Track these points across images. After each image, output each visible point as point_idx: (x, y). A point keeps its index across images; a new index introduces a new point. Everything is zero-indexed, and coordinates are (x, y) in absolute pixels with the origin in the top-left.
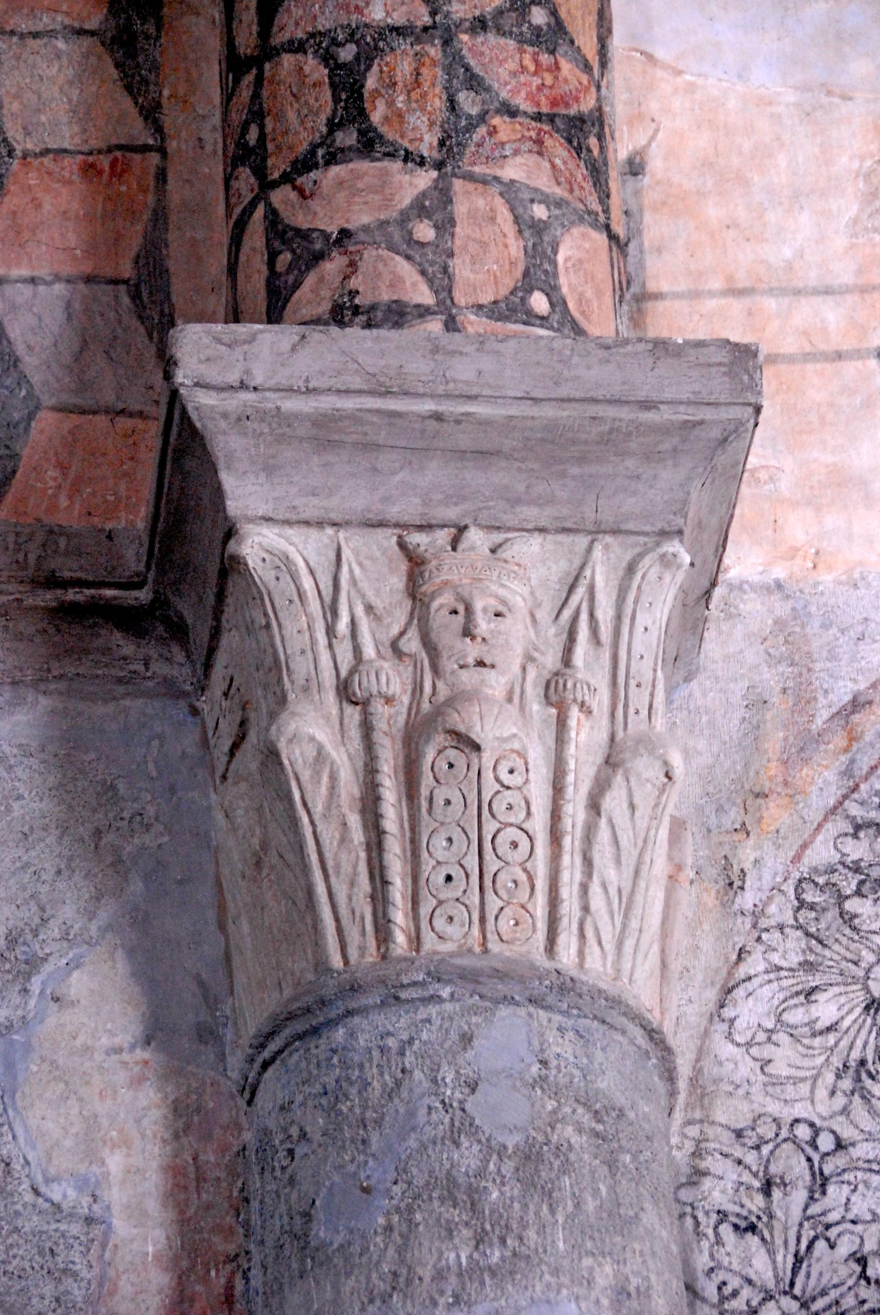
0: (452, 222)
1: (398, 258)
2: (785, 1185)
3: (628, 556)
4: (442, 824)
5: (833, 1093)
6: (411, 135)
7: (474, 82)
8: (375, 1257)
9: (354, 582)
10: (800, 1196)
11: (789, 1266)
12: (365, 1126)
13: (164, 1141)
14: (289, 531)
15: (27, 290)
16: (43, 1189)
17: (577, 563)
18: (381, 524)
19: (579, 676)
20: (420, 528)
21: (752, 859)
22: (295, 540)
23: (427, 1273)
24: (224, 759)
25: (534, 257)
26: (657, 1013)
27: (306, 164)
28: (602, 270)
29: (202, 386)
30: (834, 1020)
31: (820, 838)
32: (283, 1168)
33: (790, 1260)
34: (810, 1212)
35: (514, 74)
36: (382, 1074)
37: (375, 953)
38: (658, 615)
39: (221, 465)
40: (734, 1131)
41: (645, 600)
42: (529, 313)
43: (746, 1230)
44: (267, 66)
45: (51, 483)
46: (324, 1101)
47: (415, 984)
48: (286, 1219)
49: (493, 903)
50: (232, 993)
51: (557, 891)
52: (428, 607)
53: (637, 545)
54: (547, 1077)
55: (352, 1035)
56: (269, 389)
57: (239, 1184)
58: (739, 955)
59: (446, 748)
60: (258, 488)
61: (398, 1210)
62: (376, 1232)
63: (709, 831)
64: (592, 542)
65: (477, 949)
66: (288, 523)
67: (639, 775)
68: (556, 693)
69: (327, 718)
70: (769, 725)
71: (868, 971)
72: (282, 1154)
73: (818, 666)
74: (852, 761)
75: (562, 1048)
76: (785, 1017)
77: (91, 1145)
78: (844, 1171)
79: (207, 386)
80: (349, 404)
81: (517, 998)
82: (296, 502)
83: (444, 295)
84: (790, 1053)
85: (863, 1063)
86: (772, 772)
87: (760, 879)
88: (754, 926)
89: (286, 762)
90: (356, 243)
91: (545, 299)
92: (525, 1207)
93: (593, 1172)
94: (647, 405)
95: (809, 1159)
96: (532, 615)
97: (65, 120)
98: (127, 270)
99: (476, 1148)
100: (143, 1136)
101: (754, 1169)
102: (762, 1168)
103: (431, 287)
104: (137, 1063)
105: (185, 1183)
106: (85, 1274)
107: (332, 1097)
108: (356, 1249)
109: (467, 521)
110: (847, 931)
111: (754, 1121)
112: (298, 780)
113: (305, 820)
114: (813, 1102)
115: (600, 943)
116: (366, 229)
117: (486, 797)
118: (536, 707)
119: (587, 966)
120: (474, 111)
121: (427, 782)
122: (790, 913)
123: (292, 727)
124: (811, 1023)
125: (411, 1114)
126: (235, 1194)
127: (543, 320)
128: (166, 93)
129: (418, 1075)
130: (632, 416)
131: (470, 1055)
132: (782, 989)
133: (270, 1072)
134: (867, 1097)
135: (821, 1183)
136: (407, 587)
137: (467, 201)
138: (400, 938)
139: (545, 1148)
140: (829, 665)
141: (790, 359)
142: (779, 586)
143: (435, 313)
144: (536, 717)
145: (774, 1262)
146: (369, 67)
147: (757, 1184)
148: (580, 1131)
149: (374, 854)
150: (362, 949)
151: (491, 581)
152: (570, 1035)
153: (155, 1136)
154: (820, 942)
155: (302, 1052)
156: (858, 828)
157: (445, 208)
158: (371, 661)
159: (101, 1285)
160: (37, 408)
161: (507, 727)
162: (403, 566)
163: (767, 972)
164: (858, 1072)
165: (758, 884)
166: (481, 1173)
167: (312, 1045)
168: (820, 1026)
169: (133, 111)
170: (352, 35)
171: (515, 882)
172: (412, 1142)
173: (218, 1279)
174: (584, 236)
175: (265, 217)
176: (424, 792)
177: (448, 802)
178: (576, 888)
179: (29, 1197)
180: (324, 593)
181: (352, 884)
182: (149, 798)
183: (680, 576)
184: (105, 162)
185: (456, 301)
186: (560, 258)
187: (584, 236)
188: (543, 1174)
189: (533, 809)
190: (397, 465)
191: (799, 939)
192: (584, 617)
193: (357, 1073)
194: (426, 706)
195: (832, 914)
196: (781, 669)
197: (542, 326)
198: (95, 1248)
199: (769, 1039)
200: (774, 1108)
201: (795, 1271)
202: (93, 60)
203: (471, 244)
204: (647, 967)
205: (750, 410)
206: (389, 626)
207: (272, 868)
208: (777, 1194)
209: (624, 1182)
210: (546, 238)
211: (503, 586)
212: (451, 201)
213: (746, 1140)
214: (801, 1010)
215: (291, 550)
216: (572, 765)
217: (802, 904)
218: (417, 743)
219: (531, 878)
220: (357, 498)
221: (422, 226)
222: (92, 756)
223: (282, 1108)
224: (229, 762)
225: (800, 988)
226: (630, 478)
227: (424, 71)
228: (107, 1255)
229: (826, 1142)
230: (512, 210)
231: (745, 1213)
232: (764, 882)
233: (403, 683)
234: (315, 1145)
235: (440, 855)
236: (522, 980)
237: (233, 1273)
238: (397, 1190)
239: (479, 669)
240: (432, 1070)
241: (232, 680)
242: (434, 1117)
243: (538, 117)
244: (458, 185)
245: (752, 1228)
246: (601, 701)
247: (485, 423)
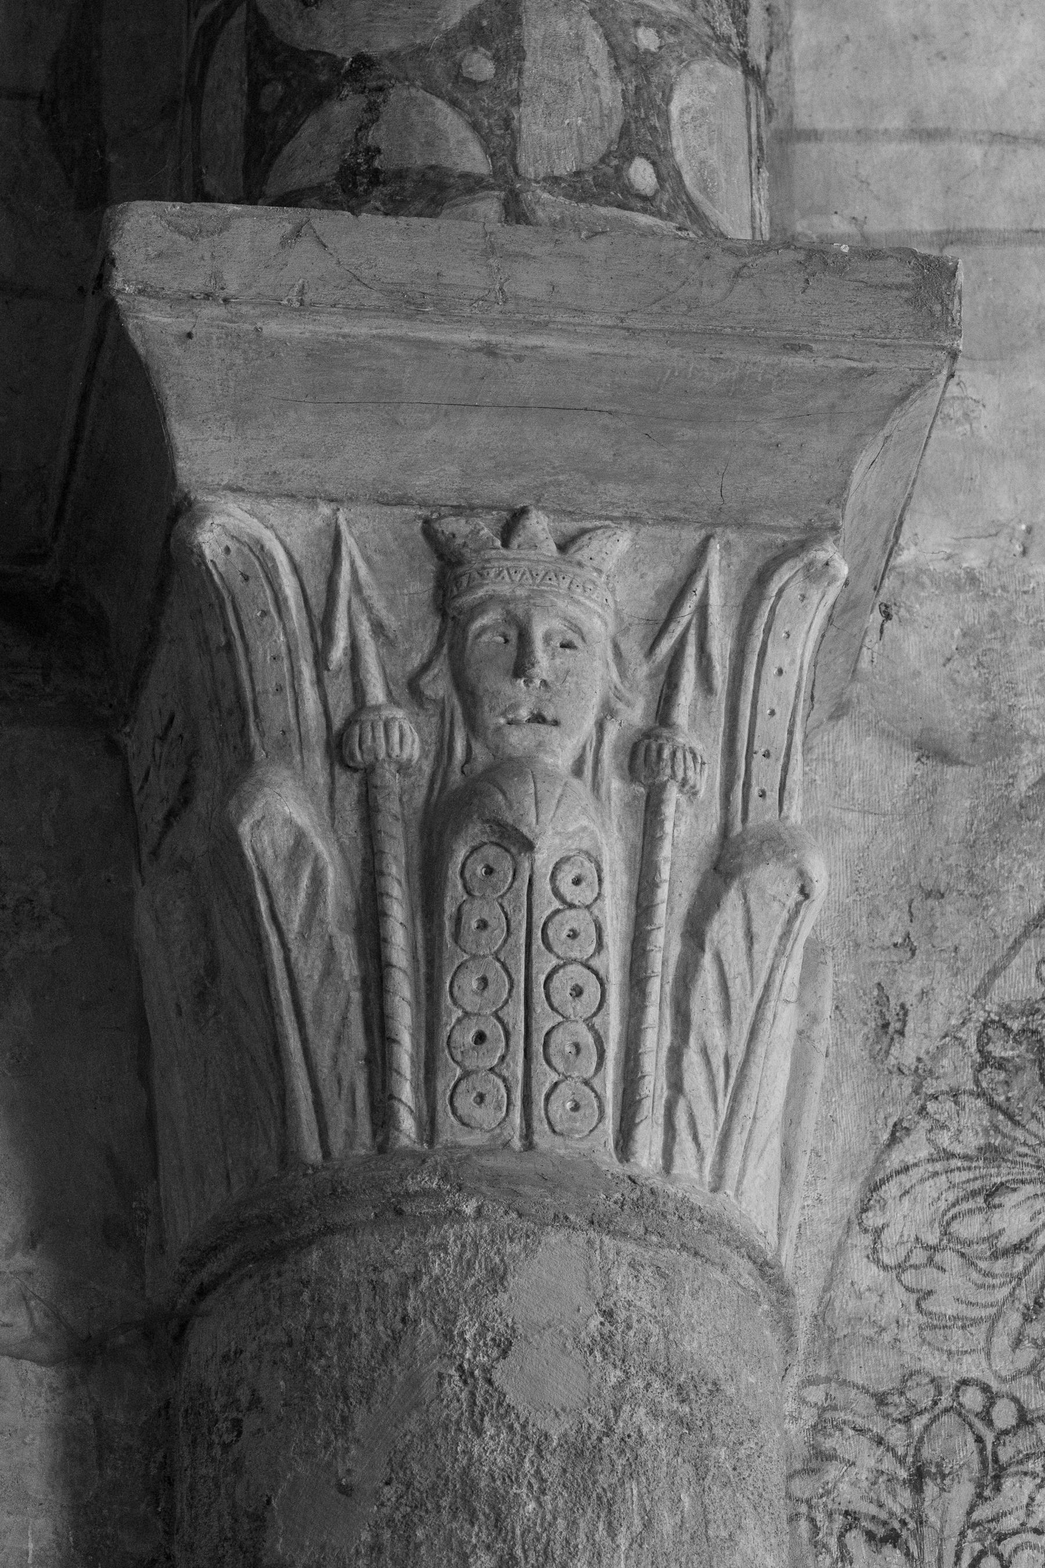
0: (520, 53)
1: (439, 104)
2: (944, 1477)
4: (474, 957)
5: (1017, 1343)
9: (357, 587)
10: (963, 1492)
12: (346, 1398)
13: (52, 1389)
14: (265, 507)
17: (683, 570)
18: (401, 502)
19: (681, 740)
20: (458, 511)
21: (917, 989)
22: (273, 520)
24: (156, 829)
25: (636, 107)
26: (773, 1238)
28: (734, 124)
30: (1025, 1234)
31: (1017, 961)
32: (226, 1447)
34: (975, 1516)
36: (373, 1322)
37: (368, 1142)
38: (799, 651)
40: (874, 1395)
41: (780, 629)
43: (884, 1540)
46: (287, 1355)
47: (425, 1193)
48: (227, 1521)
49: (544, 1077)
50: (155, 1175)
52: (465, 631)
54: (611, 1335)
55: (330, 1262)
57: (159, 1456)
58: (893, 1134)
59: (483, 844)
60: (224, 444)
62: (358, 1552)
63: (857, 945)
65: (517, 1143)
66: (264, 495)
67: (762, 891)
68: (645, 759)
69: (311, 791)
70: (950, 787)
73: (1024, 702)
76: (955, 1227)
78: (1028, 1457)
80: (362, 329)
81: (572, 1217)
82: (278, 466)
83: (504, 160)
84: (959, 1281)
86: (952, 861)
87: (928, 1020)
88: (916, 1091)
89: (249, 854)
90: (379, 77)
91: (650, 170)
92: (572, 1525)
93: (672, 1475)
95: (979, 1439)
101: (900, 1451)
102: (912, 1452)
103: (486, 149)
104: (16, 1274)
111: (904, 1381)
113: (274, 940)
114: (988, 1354)
116: (393, 56)
117: (540, 918)
118: (614, 785)
119: (675, 1171)
121: (454, 892)
125: (414, 1383)
126: (154, 1471)
127: (646, 202)
131: (502, 1299)
132: (952, 1186)
136: (435, 596)
138: (407, 1123)
139: (606, 1441)
141: (1002, 240)
142: (973, 579)
143: (490, 187)
144: (615, 798)
147: (903, 1474)
148: (655, 1414)
149: (372, 996)
150: (351, 1135)
151: (558, 595)
153: (40, 1383)
154: (1010, 1117)
155: (257, 1279)
157: (510, 32)
158: (377, 708)
161: (576, 827)
162: (431, 567)
163: (931, 1160)
165: (924, 1028)
167: (273, 1272)
172: (413, 1425)
174: (709, 73)
175: (248, 27)
176: (450, 908)
178: (664, 1053)
180: (313, 601)
181: (339, 1039)
182: (44, 876)
183: (833, 592)
185: (521, 171)
186: (674, 109)
187: (709, 73)
188: (601, 1478)
190: (427, 416)
191: (980, 1112)
192: (691, 650)
193: (336, 1317)
194: (456, 778)
196: (970, 704)
197: (644, 211)
199: (931, 1260)
200: (933, 1362)
203: (545, 85)
204: (761, 1171)
208: (931, 1489)
209: (715, 1489)
210: (655, 79)
212: (519, 22)
213: (891, 1410)
214: (979, 1218)
216: (665, 871)
217: (986, 1060)
218: (441, 834)
221: (476, 56)
223: (225, 1358)
224: (163, 834)
225: (977, 1185)
229: (1004, 1415)
230: (607, 36)
231: (883, 1515)
232: (934, 1025)
233: (423, 741)
239: (536, 726)
240: (446, 1320)
241: (172, 719)
245: (893, 1538)
246: (708, 780)
247: (557, 362)
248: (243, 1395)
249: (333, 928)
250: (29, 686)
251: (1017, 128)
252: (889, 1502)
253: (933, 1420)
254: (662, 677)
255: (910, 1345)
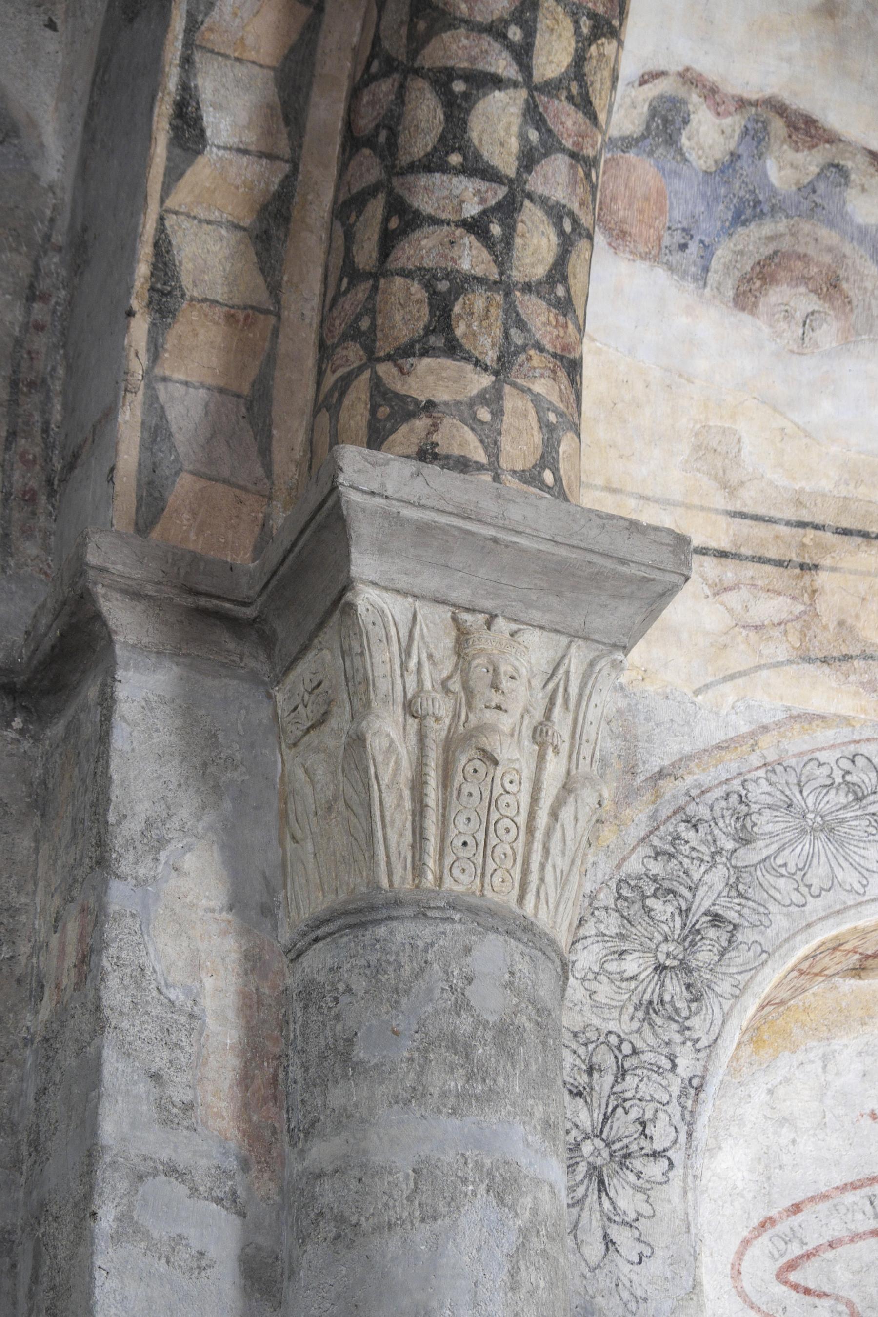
0: (502, 412)
1: (466, 428)
3: (591, 656)
5: (632, 1019)
6: (480, 349)
7: (521, 324)
8: (401, 1076)
9: (422, 637)
10: (609, 1079)
11: (601, 1121)
12: (398, 993)
14: (385, 594)
15: (182, 389)
16: (164, 990)
17: (560, 654)
18: (444, 602)
20: (468, 610)
22: (388, 601)
23: (436, 1092)
27: (407, 351)
29: (354, 488)
31: (634, 856)
33: (601, 1117)
34: (614, 1090)
35: (544, 324)
36: (411, 961)
39: (353, 543)
42: (543, 482)
43: (576, 1094)
44: (382, 281)
45: (185, 522)
46: (368, 972)
47: (437, 908)
48: (331, 1041)
49: (491, 866)
51: (528, 865)
52: (470, 663)
53: (597, 650)
56: (395, 499)
57: (283, 1010)
61: (418, 1049)
64: (571, 642)
65: (478, 893)
66: (386, 589)
67: (583, 800)
68: (540, 734)
71: (658, 946)
72: (329, 999)
73: (640, 744)
74: (657, 810)
75: (523, 966)
76: (606, 965)
77: (195, 967)
79: (357, 489)
80: (443, 519)
82: (394, 576)
85: (651, 1003)
88: (590, 905)
89: (369, 747)
94: (623, 561)
95: (616, 1057)
96: (529, 682)
97: (220, 282)
98: (246, 389)
99: (471, 1020)
100: (226, 969)
103: (486, 451)
105: (251, 1004)
106: (187, 1048)
107: (375, 971)
108: (387, 1068)
109: (498, 612)
110: (646, 918)
112: (374, 760)
115: (547, 903)
116: (446, 404)
118: (526, 743)
120: (520, 343)
121: (459, 779)
122: (612, 901)
123: (377, 725)
124: (621, 973)
125: (430, 991)
128: (285, 278)
129: (435, 966)
130: (613, 566)
132: (605, 948)
133: (320, 944)
134: (652, 1025)
135: (622, 1073)
137: (512, 401)
140: (647, 745)
142: (622, 688)
143: (487, 470)
145: (592, 1116)
146: (457, 299)
147: (584, 1067)
148: (530, 1020)
150: (403, 879)
152: (527, 958)
154: (630, 922)
156: (657, 854)
159: (198, 1058)
160: (181, 470)
161: (515, 755)
162: (454, 633)
163: (596, 935)
164: (647, 1008)
166: (472, 1036)
167: (360, 934)
168: (626, 975)
169: (263, 286)
170: (448, 274)
171: (505, 854)
173: (268, 1068)
175: (371, 379)
176: (456, 785)
177: (470, 794)
179: (155, 993)
180: (402, 640)
181: (401, 835)
184: (241, 315)
186: (561, 450)
189: (521, 810)
192: (561, 690)
195: (637, 906)
196: (618, 742)
198: (195, 1034)
200: (597, 1022)
201: (604, 1123)
202: (242, 247)
205: (683, 578)
206: (441, 671)
207: (339, 813)
208: (596, 1075)
211: (517, 659)
214: (616, 963)
215: (385, 606)
217: (620, 896)
218: (454, 752)
219: (514, 853)
220: (431, 582)
222: (203, 712)
223: (331, 969)
226: (601, 606)
227: (492, 310)
228: (203, 1040)
229: (626, 1049)
231: (576, 1084)
234: (359, 998)
235: (462, 827)
236: (503, 919)
237: (278, 1066)
238: (417, 1036)
242: (445, 995)
243: (555, 355)
244: (507, 388)
245: (580, 1094)
246: (565, 748)
247: (523, 550)
248: (341, 987)
249: (402, 786)
250: (234, 661)
251: (650, 494)
252: (579, 1079)
253: (597, 1046)
254: (547, 700)
255: (587, 1012)
